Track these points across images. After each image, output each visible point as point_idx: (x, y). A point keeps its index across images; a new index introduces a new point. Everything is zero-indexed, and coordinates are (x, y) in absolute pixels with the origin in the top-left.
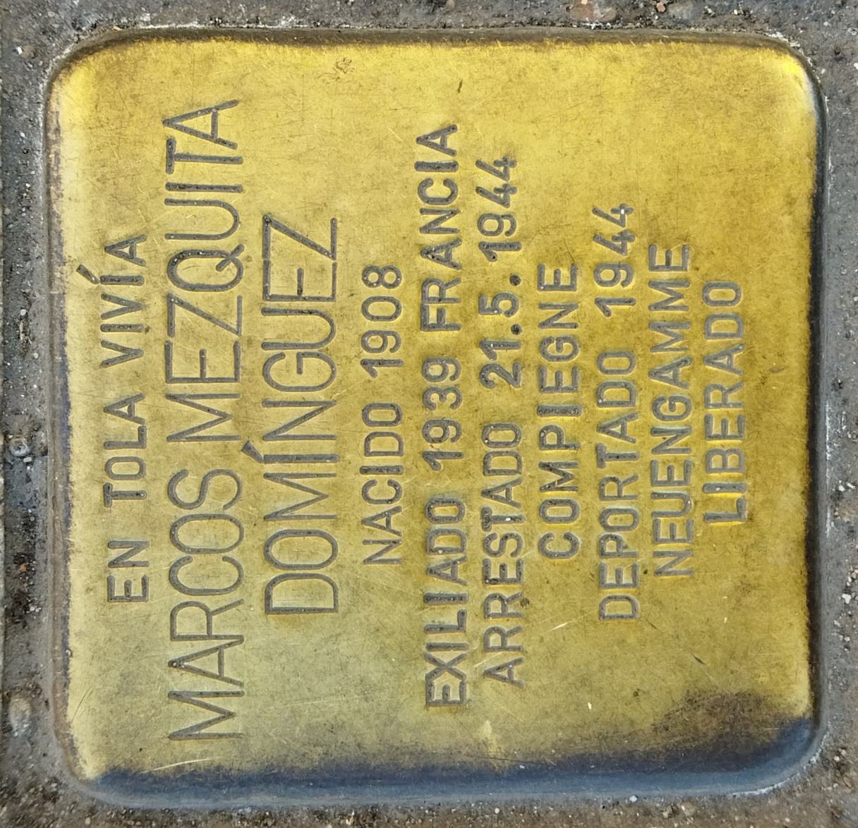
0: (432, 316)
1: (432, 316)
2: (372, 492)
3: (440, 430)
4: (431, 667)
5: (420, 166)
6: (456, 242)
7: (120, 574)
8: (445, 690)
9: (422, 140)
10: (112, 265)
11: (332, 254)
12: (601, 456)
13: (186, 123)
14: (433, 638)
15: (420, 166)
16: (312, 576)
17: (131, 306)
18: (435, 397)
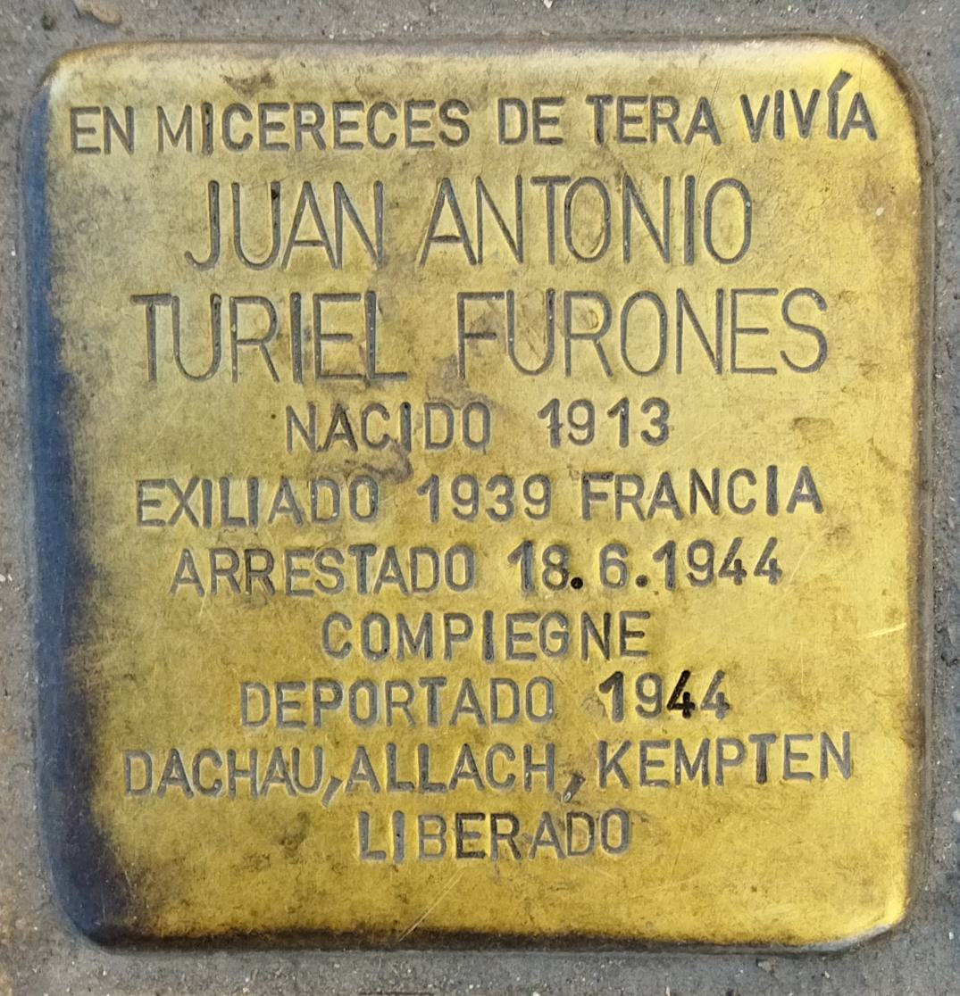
0: (596, 487)
1: (596, 487)
4: (183, 485)
5: (772, 471)
6: (679, 514)
7: (98, 121)
8: (155, 503)
9: (806, 474)
12: (435, 683)
15: (772, 471)
18: (501, 489)
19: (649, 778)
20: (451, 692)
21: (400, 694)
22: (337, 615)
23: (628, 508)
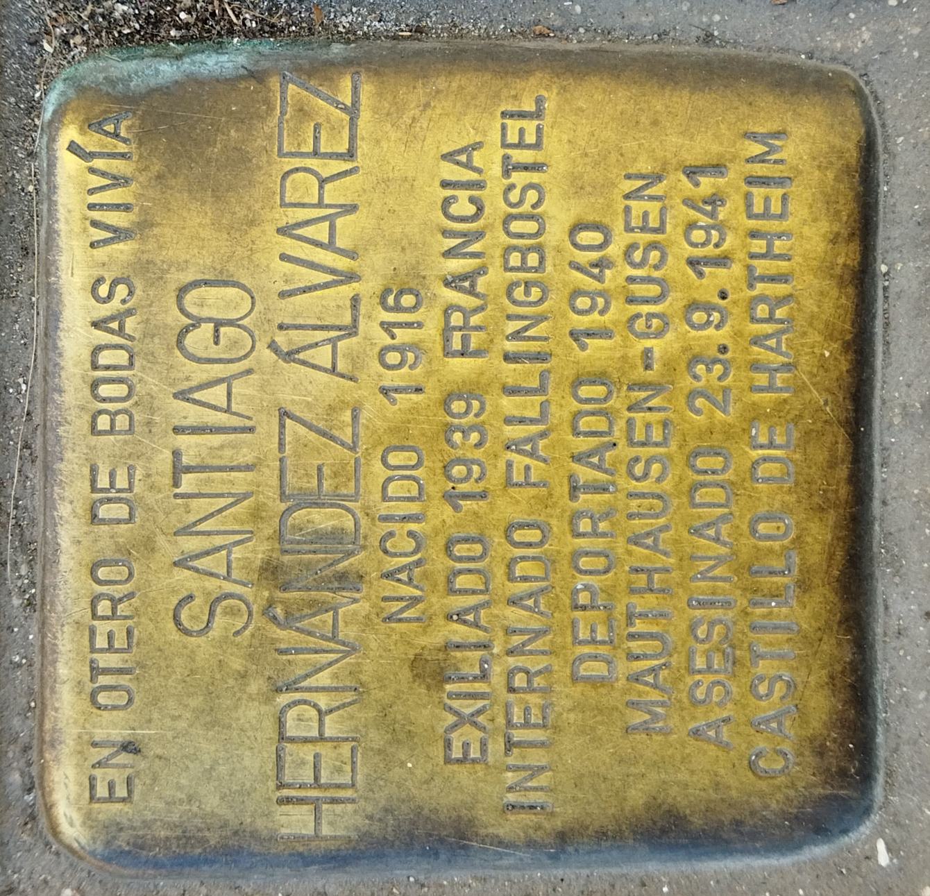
0: (456, 344)
1: (456, 344)
3: (463, 404)
4: (451, 719)
5: (445, 184)
6: (482, 271)
8: (466, 746)
9: (448, 157)
11: (353, 448)
19: (657, 225)
21: (585, 525)
22: (383, 540)
23: (475, 320)
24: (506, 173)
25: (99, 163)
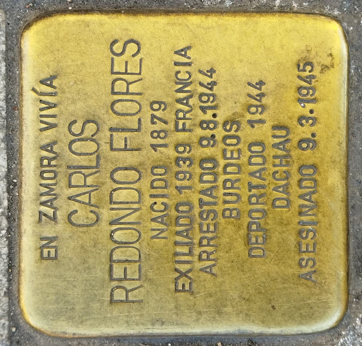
0: (180, 127)
1: (180, 127)
2: (155, 207)
4: (178, 275)
5: (176, 64)
6: (191, 96)
8: (183, 286)
10: (44, 88)
12: (251, 187)
13: (78, 198)
14: (178, 258)
15: (176, 64)
16: (130, 229)
17: (51, 106)
18: (181, 163)
20: (255, 181)
21: (254, 200)
23: (188, 116)
24: (201, 207)
25: (43, 98)
